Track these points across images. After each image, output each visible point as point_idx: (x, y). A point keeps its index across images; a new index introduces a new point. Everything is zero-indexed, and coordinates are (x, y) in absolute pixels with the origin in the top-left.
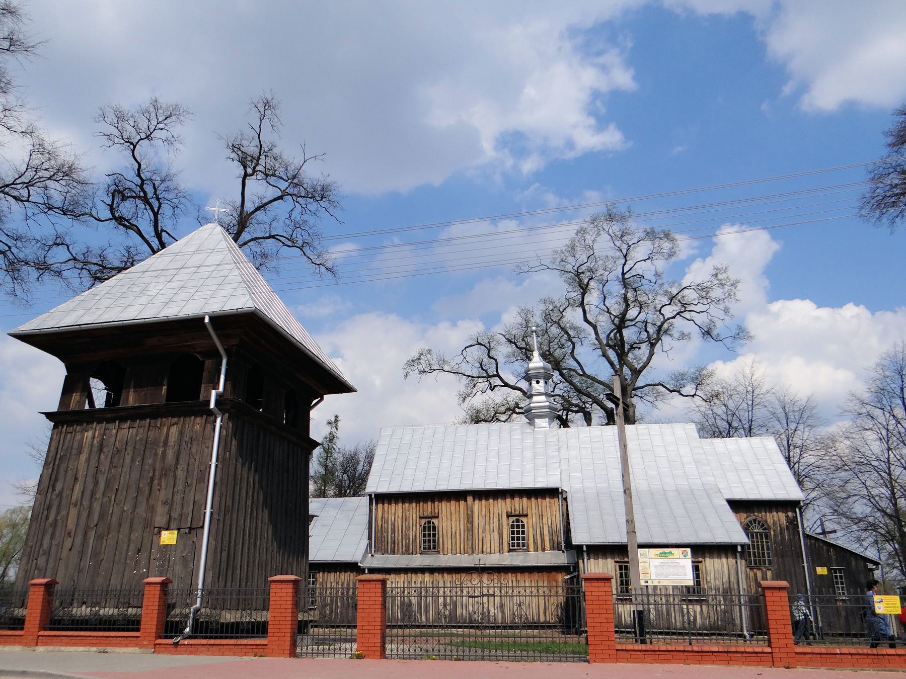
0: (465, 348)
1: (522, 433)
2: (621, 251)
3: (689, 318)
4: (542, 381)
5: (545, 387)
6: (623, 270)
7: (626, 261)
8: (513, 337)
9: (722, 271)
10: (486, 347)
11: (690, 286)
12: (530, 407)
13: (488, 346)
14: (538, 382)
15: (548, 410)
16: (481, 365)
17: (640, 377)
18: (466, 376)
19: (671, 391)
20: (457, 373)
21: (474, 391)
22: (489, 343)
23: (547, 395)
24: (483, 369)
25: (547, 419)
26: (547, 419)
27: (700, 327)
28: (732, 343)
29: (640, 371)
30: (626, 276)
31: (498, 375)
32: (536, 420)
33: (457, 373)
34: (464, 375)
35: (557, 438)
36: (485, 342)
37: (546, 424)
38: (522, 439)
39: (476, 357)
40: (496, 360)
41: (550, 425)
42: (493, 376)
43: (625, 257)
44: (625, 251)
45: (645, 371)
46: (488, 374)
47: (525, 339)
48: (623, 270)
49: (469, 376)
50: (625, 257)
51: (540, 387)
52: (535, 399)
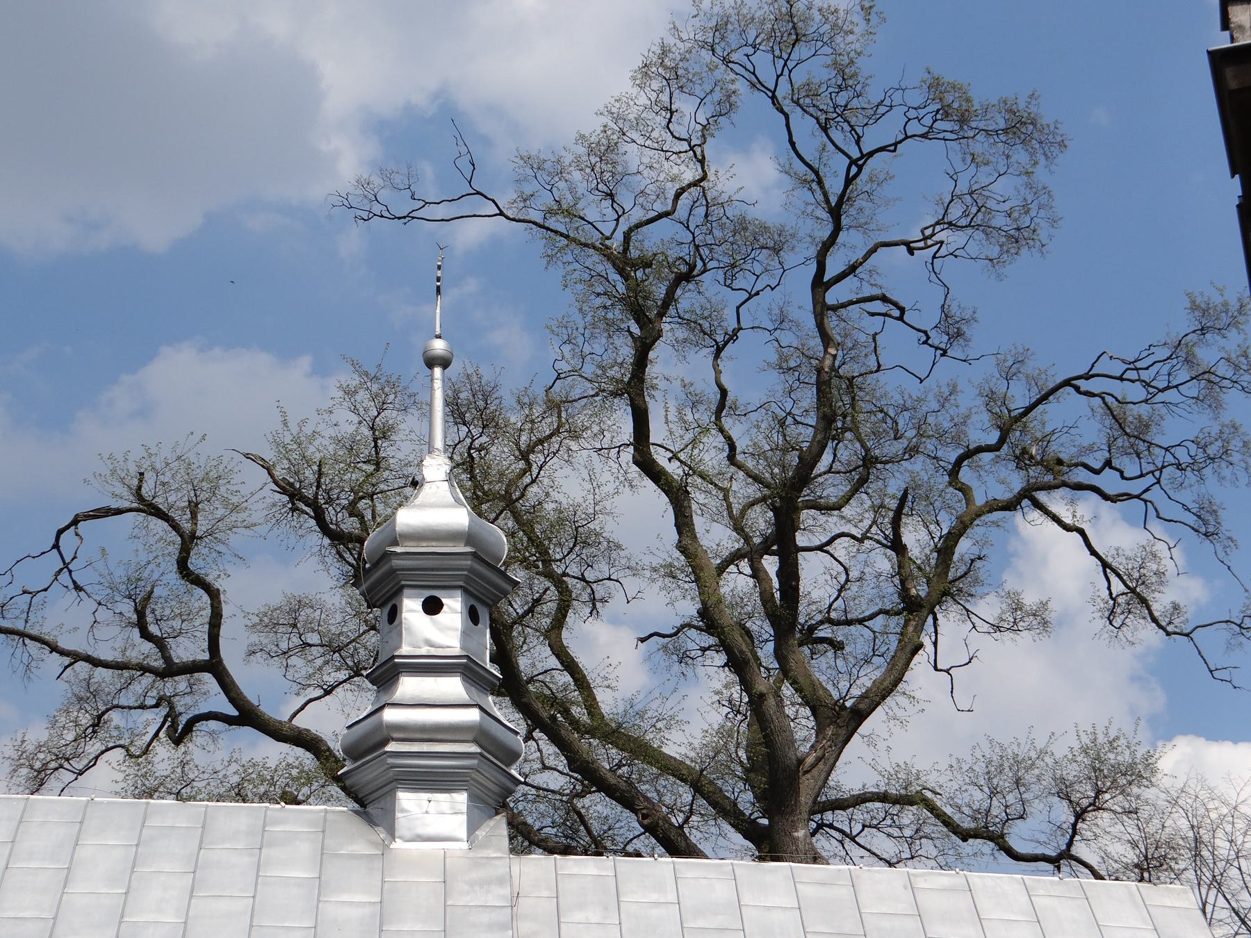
0: (75, 522)
1: (323, 856)
2: (820, 183)
3: (1068, 520)
4: (454, 605)
5: (465, 634)
6: (821, 268)
7: (837, 229)
8: (309, 475)
9: (1225, 319)
10: (175, 527)
11: (1087, 377)
12: (380, 726)
13: (187, 526)
14: (433, 607)
15: (474, 748)
16: (141, 614)
17: (856, 744)
18: (63, 653)
19: (965, 836)
20: (22, 635)
21: (94, 747)
22: (194, 508)
23: (467, 669)
24: (146, 635)
25: (461, 798)
26: (461, 798)
27: (1105, 565)
28: (1229, 647)
29: (859, 715)
30: (832, 297)
31: (214, 666)
32: (409, 802)
33: (22, 635)
34: (54, 648)
35: (506, 891)
36: (175, 500)
37: (458, 825)
38: (320, 885)
39: (120, 574)
40: (214, 594)
41: (472, 828)
42: (192, 668)
43: (836, 213)
44: (835, 186)
45: (878, 715)
46: (167, 658)
47: (362, 504)
48: (821, 268)
49: (76, 657)
50: (836, 213)
51: (443, 629)
52: (409, 686)
